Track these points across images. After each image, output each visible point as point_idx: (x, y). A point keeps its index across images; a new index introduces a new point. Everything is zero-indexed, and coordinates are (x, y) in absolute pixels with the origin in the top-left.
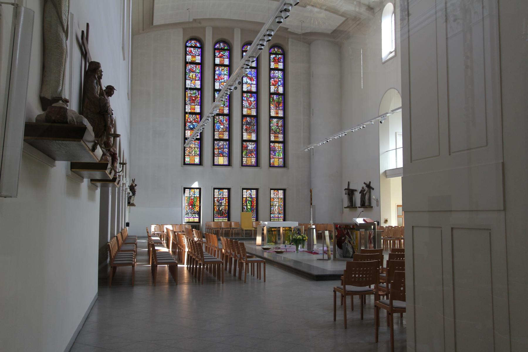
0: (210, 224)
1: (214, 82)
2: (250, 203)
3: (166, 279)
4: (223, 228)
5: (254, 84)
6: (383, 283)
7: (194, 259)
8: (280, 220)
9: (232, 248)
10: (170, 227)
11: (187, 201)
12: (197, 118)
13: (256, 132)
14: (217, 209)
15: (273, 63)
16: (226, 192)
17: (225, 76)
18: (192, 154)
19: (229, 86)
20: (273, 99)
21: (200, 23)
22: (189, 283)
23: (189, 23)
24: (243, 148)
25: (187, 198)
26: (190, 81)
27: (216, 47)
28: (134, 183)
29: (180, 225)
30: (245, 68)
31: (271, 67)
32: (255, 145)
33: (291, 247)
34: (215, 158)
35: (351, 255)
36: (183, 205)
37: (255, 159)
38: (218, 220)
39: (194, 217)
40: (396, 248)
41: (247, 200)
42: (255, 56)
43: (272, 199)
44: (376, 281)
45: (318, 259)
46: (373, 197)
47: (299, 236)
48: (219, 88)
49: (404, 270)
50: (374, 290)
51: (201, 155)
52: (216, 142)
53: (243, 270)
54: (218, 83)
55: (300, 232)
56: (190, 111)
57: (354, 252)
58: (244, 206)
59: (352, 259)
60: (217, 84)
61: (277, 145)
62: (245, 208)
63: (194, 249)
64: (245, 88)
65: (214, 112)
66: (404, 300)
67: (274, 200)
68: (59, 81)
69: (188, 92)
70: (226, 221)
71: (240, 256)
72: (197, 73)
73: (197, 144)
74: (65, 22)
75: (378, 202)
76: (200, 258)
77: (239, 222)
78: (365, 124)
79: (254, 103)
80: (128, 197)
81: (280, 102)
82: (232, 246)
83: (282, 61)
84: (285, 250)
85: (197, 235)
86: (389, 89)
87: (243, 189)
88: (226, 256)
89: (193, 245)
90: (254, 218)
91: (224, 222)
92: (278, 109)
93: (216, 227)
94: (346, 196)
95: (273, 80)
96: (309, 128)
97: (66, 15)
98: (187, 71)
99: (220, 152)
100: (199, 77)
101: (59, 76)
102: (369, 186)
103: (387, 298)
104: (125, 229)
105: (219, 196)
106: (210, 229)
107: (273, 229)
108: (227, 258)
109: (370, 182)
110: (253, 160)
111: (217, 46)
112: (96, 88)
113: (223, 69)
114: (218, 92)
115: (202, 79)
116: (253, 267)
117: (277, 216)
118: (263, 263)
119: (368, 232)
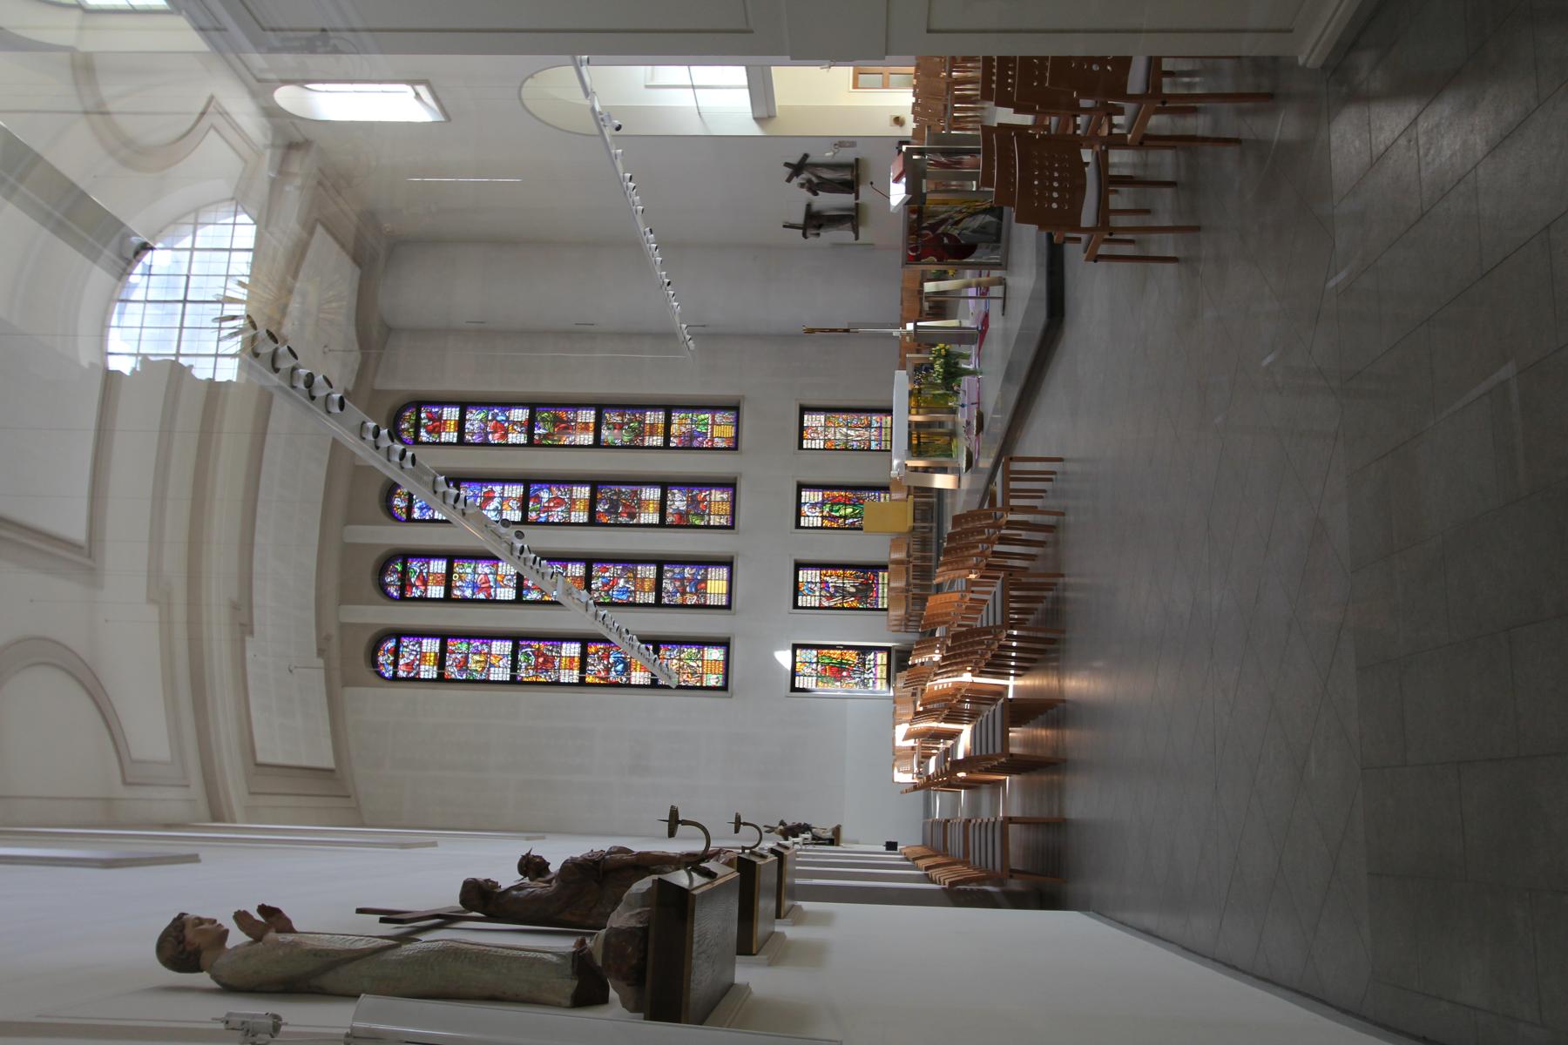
0: (896, 620)
1: (496, 601)
2: (837, 508)
3: (1047, 736)
4: (908, 584)
5: (503, 489)
6: (1077, 127)
7: (993, 656)
8: (889, 422)
9: (967, 549)
10: (901, 730)
11: (827, 683)
12: (597, 652)
13: (639, 487)
14: (853, 599)
15: (443, 434)
16: (804, 575)
17: (480, 570)
18: (698, 666)
19: (512, 554)
20: (546, 436)
21: (328, 638)
22: (1060, 672)
23: (328, 670)
24: (683, 524)
25: (820, 684)
26: (492, 669)
27: (395, 594)
28: (777, 828)
29: (895, 702)
30: (463, 507)
31: (455, 440)
32: (676, 491)
33: (965, 391)
34: (708, 603)
35: (993, 219)
36: (838, 693)
37: (713, 491)
38: (883, 597)
39: (875, 665)
40: (979, 92)
41: (830, 516)
42: (431, 478)
43: (829, 445)
44: (1076, 144)
45: (1003, 314)
46: (828, 155)
47: (937, 367)
48: (511, 590)
49: (1043, 59)
50: (1097, 148)
51: (702, 643)
52: (665, 600)
53: (1020, 535)
54: (498, 590)
55: (922, 364)
56: (576, 672)
57: (985, 211)
58: (845, 524)
59: (1006, 209)
60: (502, 595)
61: (674, 429)
62: (851, 521)
63: (966, 654)
64: (513, 515)
65: (584, 600)
66: (1124, 63)
67: (829, 439)
68: (530, 958)
69: (522, 674)
70: (886, 574)
71: (989, 526)
72: (468, 649)
73: (668, 653)
74: (374, 942)
75: (842, 143)
76: (991, 637)
77: (892, 540)
78: (621, 175)
79: (556, 491)
80: (815, 844)
81: (555, 415)
82: (961, 549)
83: (436, 410)
84: (975, 406)
85: (925, 654)
86: (523, 105)
87: (798, 525)
88: (993, 557)
89: (954, 656)
90: (879, 498)
91: (889, 580)
92: (573, 424)
93: (904, 603)
94: (823, 233)
95: (490, 437)
96: (628, 336)
97: (356, 940)
98: (464, 677)
99: (693, 590)
100: (482, 644)
101: (516, 958)
102: (797, 169)
103: (1120, 112)
104: (904, 851)
105: (817, 593)
106: (911, 616)
107: (915, 442)
108: (990, 570)
109: (787, 165)
110: (717, 495)
111: (394, 591)
112: (533, 892)
113: (460, 577)
114: (524, 592)
115: (488, 637)
116: (1020, 494)
117: (876, 433)
118: (1012, 463)
119: (930, 169)
